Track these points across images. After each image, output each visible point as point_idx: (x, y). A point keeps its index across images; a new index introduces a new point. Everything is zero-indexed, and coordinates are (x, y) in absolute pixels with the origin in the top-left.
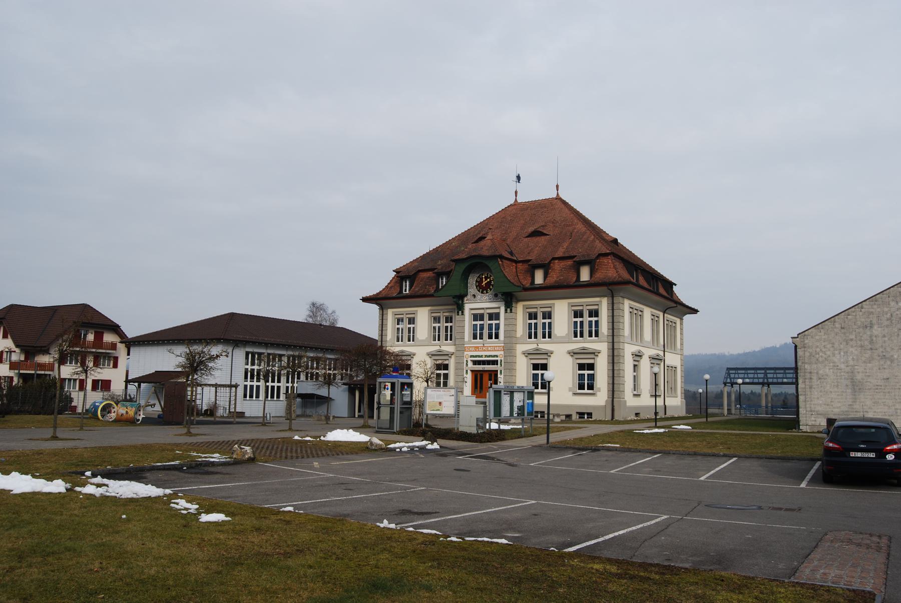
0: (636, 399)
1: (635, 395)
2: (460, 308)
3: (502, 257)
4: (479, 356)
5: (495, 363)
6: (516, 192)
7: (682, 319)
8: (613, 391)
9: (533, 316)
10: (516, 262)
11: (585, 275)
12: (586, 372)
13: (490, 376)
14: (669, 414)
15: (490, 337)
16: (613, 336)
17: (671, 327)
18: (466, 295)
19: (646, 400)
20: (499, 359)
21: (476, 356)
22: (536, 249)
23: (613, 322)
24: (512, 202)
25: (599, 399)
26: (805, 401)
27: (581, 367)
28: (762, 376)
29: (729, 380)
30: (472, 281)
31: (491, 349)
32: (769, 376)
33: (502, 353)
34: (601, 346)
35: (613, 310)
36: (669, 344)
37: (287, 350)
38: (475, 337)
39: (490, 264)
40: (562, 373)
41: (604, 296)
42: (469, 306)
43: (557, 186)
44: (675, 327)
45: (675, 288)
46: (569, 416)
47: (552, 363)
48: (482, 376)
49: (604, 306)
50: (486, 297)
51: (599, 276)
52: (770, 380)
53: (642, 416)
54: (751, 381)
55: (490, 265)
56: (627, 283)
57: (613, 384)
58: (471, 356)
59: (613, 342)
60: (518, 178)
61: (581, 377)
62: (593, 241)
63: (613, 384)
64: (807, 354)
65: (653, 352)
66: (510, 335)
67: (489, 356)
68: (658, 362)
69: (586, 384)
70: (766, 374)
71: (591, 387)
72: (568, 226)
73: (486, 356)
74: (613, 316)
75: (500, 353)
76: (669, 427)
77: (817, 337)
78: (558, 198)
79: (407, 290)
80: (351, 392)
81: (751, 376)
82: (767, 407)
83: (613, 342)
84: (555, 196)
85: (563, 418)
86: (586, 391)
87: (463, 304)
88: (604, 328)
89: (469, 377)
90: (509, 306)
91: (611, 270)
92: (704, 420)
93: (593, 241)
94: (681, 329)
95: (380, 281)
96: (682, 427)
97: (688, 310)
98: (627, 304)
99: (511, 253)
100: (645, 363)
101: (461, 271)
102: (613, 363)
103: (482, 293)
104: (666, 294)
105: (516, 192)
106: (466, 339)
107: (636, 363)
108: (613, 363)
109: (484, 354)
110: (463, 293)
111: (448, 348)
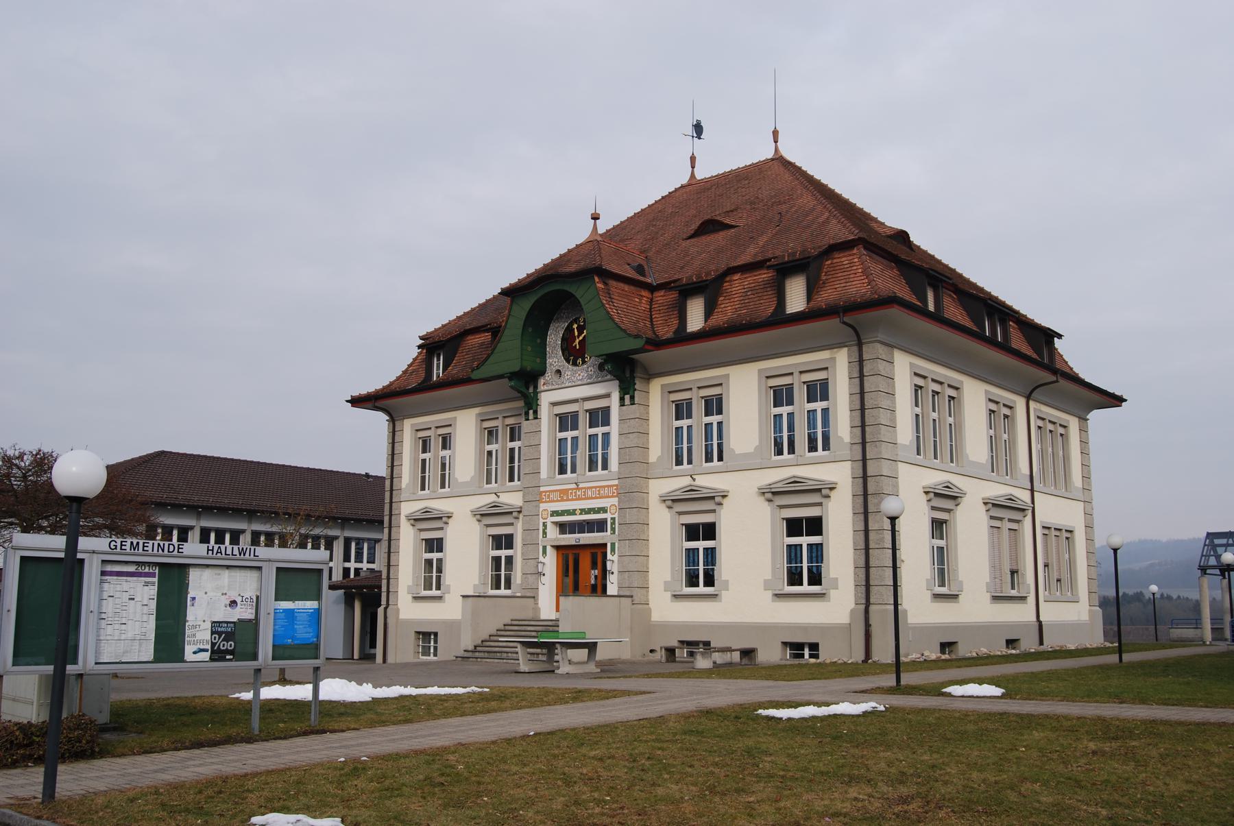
1: (937, 597)
2: (531, 405)
3: (605, 275)
4: (569, 513)
5: (600, 526)
6: (693, 159)
8: (868, 586)
10: (652, 289)
11: (796, 298)
12: (805, 541)
15: (592, 466)
16: (864, 443)
18: (543, 373)
20: (608, 516)
21: (563, 513)
22: (703, 257)
23: (863, 409)
25: (833, 609)
27: (794, 527)
29: (1213, 561)
30: (554, 338)
31: (594, 494)
33: (615, 501)
34: (838, 473)
35: (862, 376)
37: (199, 516)
38: (562, 470)
40: (750, 543)
41: (840, 345)
42: (549, 397)
45: (1057, 343)
46: (670, 651)
47: (727, 521)
51: (827, 296)
53: (963, 650)
57: (867, 567)
58: (554, 513)
59: (864, 460)
60: (698, 129)
61: (793, 551)
62: (827, 221)
63: (867, 567)
65: (997, 491)
66: (635, 458)
67: (589, 511)
68: (1016, 515)
69: (803, 571)
71: (815, 579)
72: (780, 203)
73: (583, 511)
74: (862, 393)
75: (611, 502)
76: (936, 691)
78: (779, 160)
79: (438, 371)
80: (349, 601)
83: (864, 460)
84: (770, 155)
85: (736, 656)
86: (806, 588)
87: (536, 393)
89: (550, 563)
90: (627, 389)
91: (856, 277)
93: (827, 221)
94: (1084, 443)
95: (393, 359)
96: (972, 689)
97: (1097, 398)
98: (903, 368)
100: (971, 524)
101: (523, 315)
102: (866, 513)
103: (575, 364)
104: (1035, 356)
105: (693, 159)
106: (544, 474)
108: (866, 513)
111: (513, 499)
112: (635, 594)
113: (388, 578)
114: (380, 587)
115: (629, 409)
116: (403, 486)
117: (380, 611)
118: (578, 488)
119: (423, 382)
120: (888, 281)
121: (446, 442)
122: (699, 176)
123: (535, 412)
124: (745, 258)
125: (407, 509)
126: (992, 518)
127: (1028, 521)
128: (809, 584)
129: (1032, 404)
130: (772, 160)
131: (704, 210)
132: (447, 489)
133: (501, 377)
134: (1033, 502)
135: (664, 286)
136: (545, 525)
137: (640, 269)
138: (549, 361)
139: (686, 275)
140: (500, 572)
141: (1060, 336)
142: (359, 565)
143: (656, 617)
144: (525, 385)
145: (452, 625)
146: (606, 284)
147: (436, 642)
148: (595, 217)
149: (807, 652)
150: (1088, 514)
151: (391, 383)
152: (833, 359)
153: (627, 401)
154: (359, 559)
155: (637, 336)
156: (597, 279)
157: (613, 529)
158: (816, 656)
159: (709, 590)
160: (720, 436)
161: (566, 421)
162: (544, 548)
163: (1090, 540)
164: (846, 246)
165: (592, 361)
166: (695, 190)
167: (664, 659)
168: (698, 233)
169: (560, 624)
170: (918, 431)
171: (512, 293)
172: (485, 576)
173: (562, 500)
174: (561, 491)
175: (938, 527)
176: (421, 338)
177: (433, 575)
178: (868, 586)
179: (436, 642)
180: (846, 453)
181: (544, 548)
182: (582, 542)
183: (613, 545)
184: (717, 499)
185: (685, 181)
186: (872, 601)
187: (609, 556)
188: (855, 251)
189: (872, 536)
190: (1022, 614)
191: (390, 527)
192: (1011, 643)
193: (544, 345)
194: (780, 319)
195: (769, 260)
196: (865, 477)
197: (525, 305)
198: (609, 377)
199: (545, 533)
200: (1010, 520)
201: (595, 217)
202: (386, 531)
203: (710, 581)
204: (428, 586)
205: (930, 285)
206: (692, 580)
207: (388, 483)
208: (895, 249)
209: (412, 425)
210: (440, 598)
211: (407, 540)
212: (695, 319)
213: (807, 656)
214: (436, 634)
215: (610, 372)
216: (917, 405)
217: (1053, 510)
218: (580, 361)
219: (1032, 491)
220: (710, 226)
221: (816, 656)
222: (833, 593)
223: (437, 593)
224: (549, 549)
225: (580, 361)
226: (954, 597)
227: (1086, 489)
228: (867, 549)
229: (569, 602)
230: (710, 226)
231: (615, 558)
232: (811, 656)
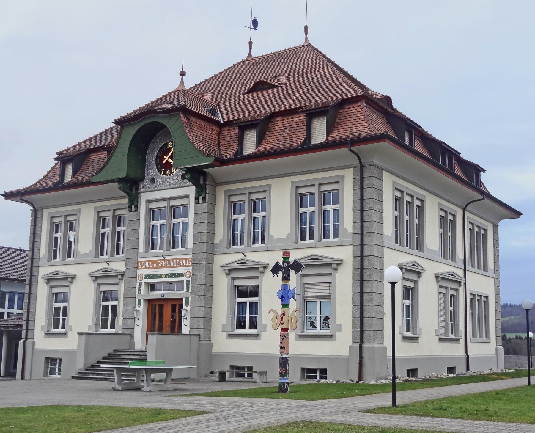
0: (413, 345)
6: (250, 43)
8: (362, 331)
13: (174, 307)
14: (474, 369)
17: (478, 238)
18: (142, 179)
30: (152, 157)
33: (190, 269)
35: (362, 188)
39: (170, 124)
43: (306, 28)
44: (485, 236)
45: (483, 177)
48: (161, 307)
51: (338, 134)
57: (362, 317)
58: (147, 277)
59: (362, 245)
60: (255, 23)
63: (362, 317)
65: (444, 269)
67: (172, 275)
68: (455, 286)
73: (167, 276)
74: (362, 199)
78: (309, 47)
83: (362, 245)
84: (302, 42)
88: (348, 222)
89: (142, 309)
90: (200, 191)
95: (37, 167)
105: (250, 43)
107: (410, 284)
111: (119, 266)
112: (203, 335)
113: (28, 320)
114: (21, 326)
116: (41, 256)
117: (21, 342)
118: (165, 260)
119: (58, 183)
120: (379, 126)
121: (71, 226)
122: (254, 55)
123: (136, 207)
124: (285, 107)
125: (43, 271)
126: (441, 287)
127: (461, 290)
128: (250, 328)
129: (466, 213)
130: (303, 46)
131: (258, 76)
132: (72, 259)
133: (112, 181)
134: (465, 277)
135: (228, 124)
136: (140, 284)
137: (213, 112)
138: (147, 171)
139: (244, 116)
140: (106, 315)
141: (484, 171)
142: (11, 311)
143: (216, 349)
144: (131, 186)
145: (71, 353)
146: (188, 119)
147: (60, 365)
148: (183, 74)
149: (318, 375)
150: (497, 287)
151: (35, 184)
152: (343, 177)
153: (201, 200)
154: (11, 307)
155: (209, 156)
156: (182, 115)
157: (188, 289)
158: (325, 378)
159: (253, 331)
160: (263, 227)
162: (139, 300)
163: (497, 302)
164: (354, 100)
165: (177, 172)
166: (252, 63)
167: (218, 379)
168: (252, 90)
169: (147, 353)
170: (396, 228)
171: (121, 122)
172: (97, 320)
173: (153, 268)
174: (153, 261)
175: (409, 293)
176: (58, 153)
177: (59, 318)
178: (362, 331)
179: (60, 365)
180: (350, 240)
181: (139, 300)
182: (165, 297)
183: (187, 299)
185: (244, 58)
186: (364, 340)
187: (184, 307)
188: (359, 104)
189: (365, 297)
190: (456, 350)
191: (30, 284)
192: (451, 370)
193: (143, 160)
194: (307, 147)
195: (302, 108)
196: (362, 257)
197: (131, 132)
198: (189, 183)
199: (140, 290)
200: (451, 289)
201: (183, 74)
202: (27, 287)
203: (253, 326)
204: (56, 326)
205: (407, 130)
206: (241, 325)
207: (30, 254)
208: (382, 106)
209: (49, 214)
210: (65, 334)
211: (42, 292)
212: (250, 146)
213: (318, 378)
214: (60, 360)
215: (189, 180)
216: (396, 210)
217: (478, 283)
218: (168, 172)
219: (465, 270)
220: (260, 86)
221: (325, 378)
222: (337, 335)
223: (63, 331)
224: (142, 301)
225: (168, 172)
226: (416, 339)
227: (496, 270)
228: (362, 305)
229: (153, 338)
230: (260, 86)
231: (189, 308)
232: (321, 378)
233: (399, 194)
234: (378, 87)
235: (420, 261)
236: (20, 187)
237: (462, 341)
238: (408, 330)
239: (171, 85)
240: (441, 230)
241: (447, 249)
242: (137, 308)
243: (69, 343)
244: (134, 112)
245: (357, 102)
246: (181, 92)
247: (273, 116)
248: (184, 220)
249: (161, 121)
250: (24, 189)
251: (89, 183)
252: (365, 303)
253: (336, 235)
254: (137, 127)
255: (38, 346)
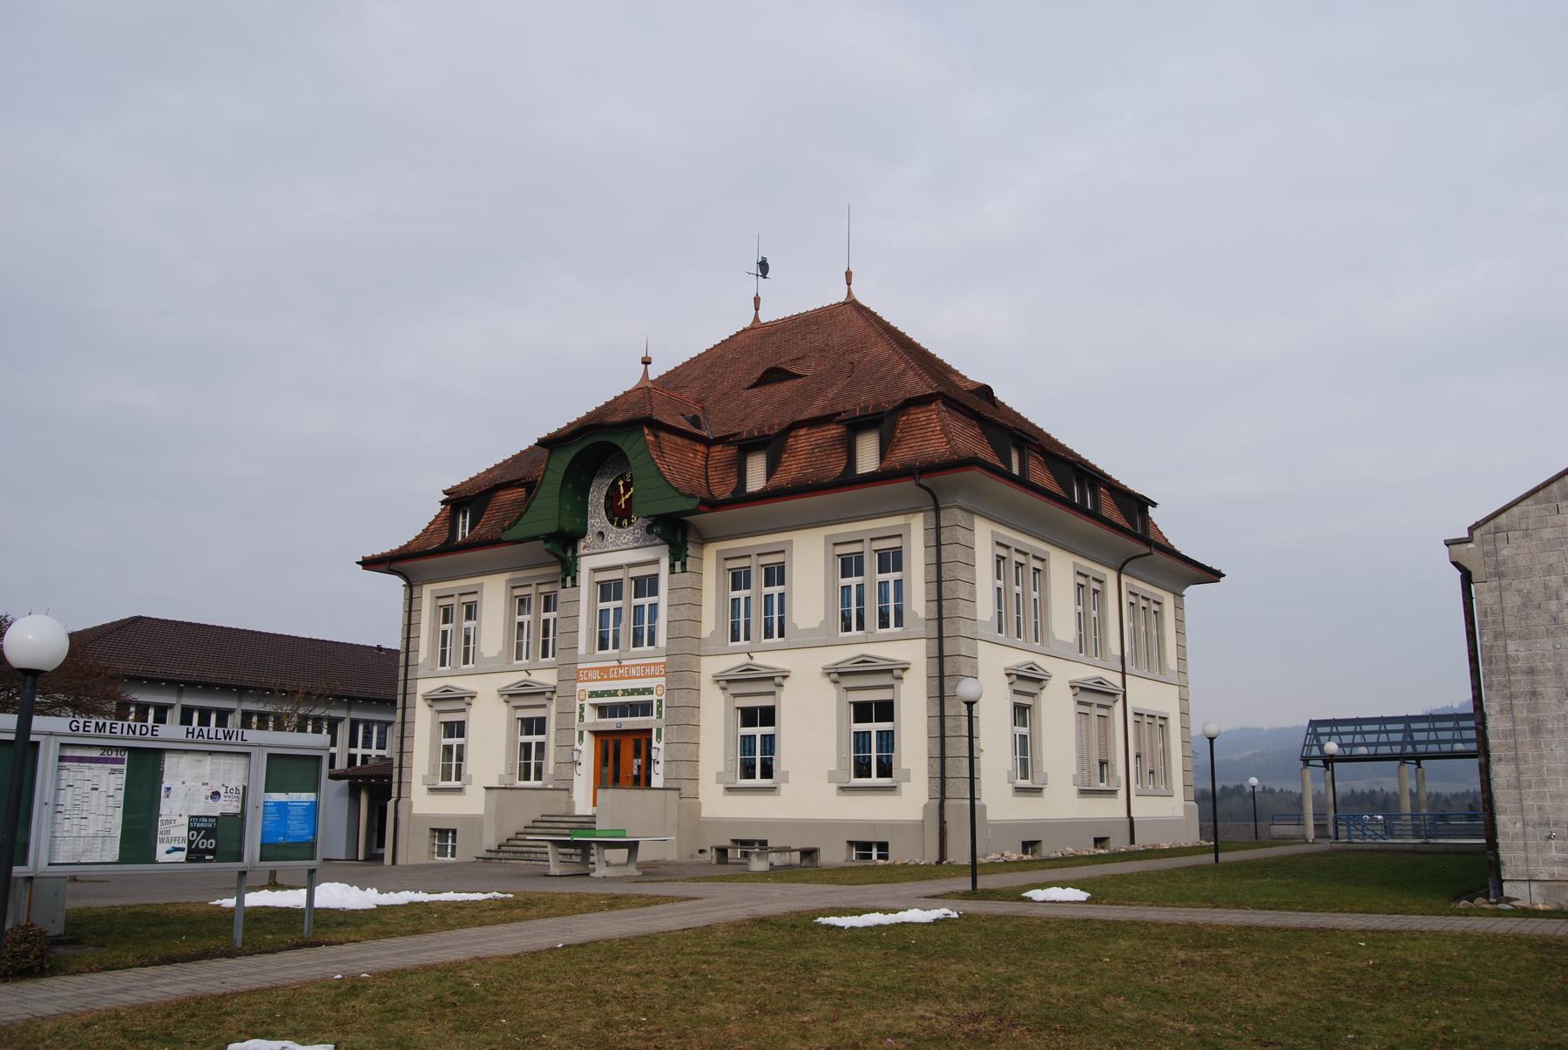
2: (569, 571)
3: (657, 426)
5: (645, 709)
6: (757, 300)
7: (1179, 596)
9: (740, 579)
10: (708, 443)
12: (874, 727)
14: (1142, 841)
15: (637, 641)
16: (940, 619)
18: (583, 535)
19: (1062, 804)
20: (654, 698)
22: (764, 409)
23: (939, 581)
24: (748, 324)
25: (904, 804)
26: (1518, 786)
27: (862, 712)
28: (1399, 737)
29: (1315, 751)
30: (597, 496)
31: (638, 672)
32: (1417, 736)
34: (913, 652)
35: (939, 545)
36: (1145, 653)
37: (180, 692)
38: (603, 645)
39: (626, 444)
43: (848, 275)
47: (788, 705)
49: (916, 530)
50: (627, 535)
52: (1421, 748)
53: (1048, 850)
54: (1372, 750)
55: (625, 448)
56: (972, 462)
58: (593, 694)
59: (940, 638)
60: (764, 267)
61: (861, 740)
62: (903, 373)
63: (943, 757)
64: (1513, 600)
65: (1085, 673)
69: (872, 761)
70: (1408, 732)
71: (885, 770)
73: (626, 692)
74: (939, 564)
77: (1547, 534)
78: (852, 304)
81: (1371, 738)
82: (1414, 816)
83: (940, 638)
84: (842, 298)
86: (875, 780)
87: (575, 558)
88: (918, 600)
89: (587, 751)
90: (678, 556)
91: (934, 436)
92: (1210, 858)
93: (903, 373)
94: (1179, 621)
95: (412, 515)
96: (1055, 893)
98: (984, 536)
99: (695, 421)
103: (620, 526)
106: (582, 649)
108: (942, 697)
109: (620, 687)
110: (567, 527)
111: (545, 677)
112: (683, 786)
114: (390, 777)
115: (680, 578)
117: (391, 804)
121: (471, 611)
122: (763, 319)
123: (574, 579)
125: (424, 687)
126: (1080, 703)
127: (1119, 707)
129: (1124, 578)
136: (582, 707)
139: (747, 428)
140: (529, 761)
141: (1154, 505)
142: (367, 752)
143: (706, 812)
144: (563, 548)
145: (473, 821)
146: (656, 436)
147: (454, 840)
148: (646, 362)
149: (875, 853)
150: (1183, 700)
155: (690, 496)
157: (659, 713)
159: (767, 782)
160: (781, 610)
161: (609, 590)
162: (581, 733)
163: (1185, 728)
166: (758, 335)
170: (999, 607)
171: (550, 444)
173: (602, 679)
174: (601, 669)
176: (445, 492)
177: (452, 763)
179: (454, 840)
180: (921, 630)
181: (581, 733)
183: (659, 730)
184: (777, 680)
187: (654, 743)
190: (1110, 810)
192: (1099, 841)
194: (850, 480)
196: (941, 657)
197: (565, 458)
199: (581, 717)
202: (399, 712)
203: (767, 772)
205: (1016, 446)
207: (402, 657)
208: (977, 405)
210: (459, 790)
213: (875, 857)
214: (454, 832)
215: (659, 535)
217: (1145, 694)
218: (625, 522)
219: (1123, 673)
221: (885, 857)
225: (625, 522)
227: (1182, 672)
228: (943, 737)
229: (607, 795)
231: (661, 745)
232: (880, 857)
233: (1002, 552)
234: (973, 370)
235: (1041, 661)
236: (386, 549)
237: (1122, 793)
238: (1025, 777)
239: (626, 380)
240: (1080, 608)
241: (1089, 636)
242: (577, 746)
243: (470, 804)
244: (569, 425)
245: (930, 402)
246: (645, 391)
247: (796, 425)
248: (652, 600)
249: (613, 440)
250: (393, 552)
251: (497, 542)
252: (948, 733)
253: (899, 623)
254: (574, 451)
255: (417, 809)
